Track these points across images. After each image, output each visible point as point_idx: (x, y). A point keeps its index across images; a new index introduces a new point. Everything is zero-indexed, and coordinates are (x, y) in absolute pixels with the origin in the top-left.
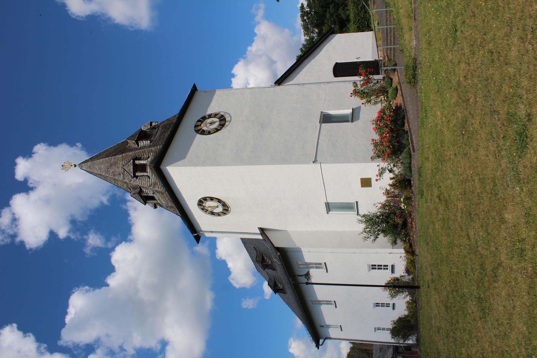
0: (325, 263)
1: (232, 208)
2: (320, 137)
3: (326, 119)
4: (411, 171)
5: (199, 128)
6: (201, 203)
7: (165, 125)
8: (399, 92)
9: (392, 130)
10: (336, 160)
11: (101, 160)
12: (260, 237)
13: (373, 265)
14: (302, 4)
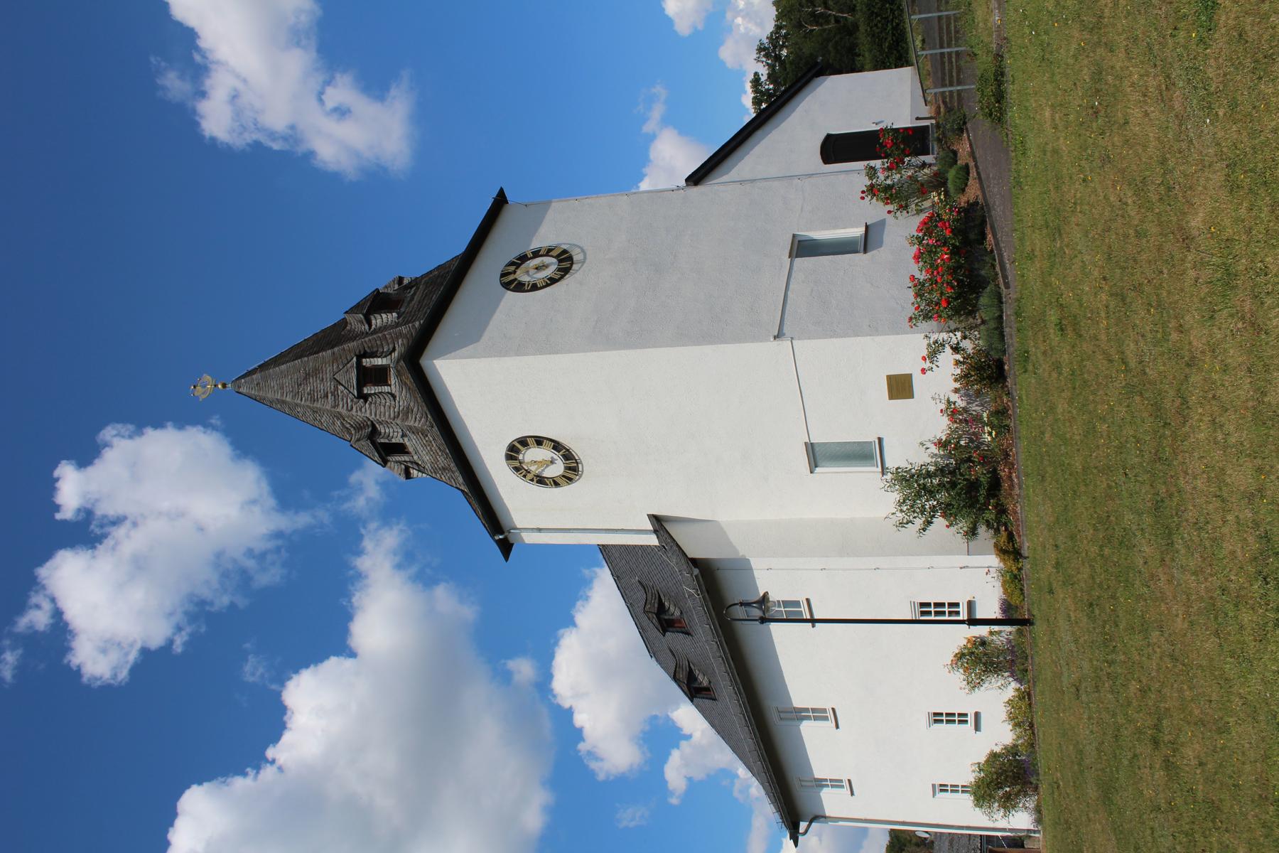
0: (808, 600)
1: (587, 465)
2: (791, 286)
3: (803, 248)
4: (1002, 336)
5: (511, 277)
6: (513, 452)
7: (431, 279)
8: (973, 174)
9: (955, 252)
10: (827, 329)
11: (283, 367)
12: (653, 540)
13: (935, 714)
14: (756, 74)
